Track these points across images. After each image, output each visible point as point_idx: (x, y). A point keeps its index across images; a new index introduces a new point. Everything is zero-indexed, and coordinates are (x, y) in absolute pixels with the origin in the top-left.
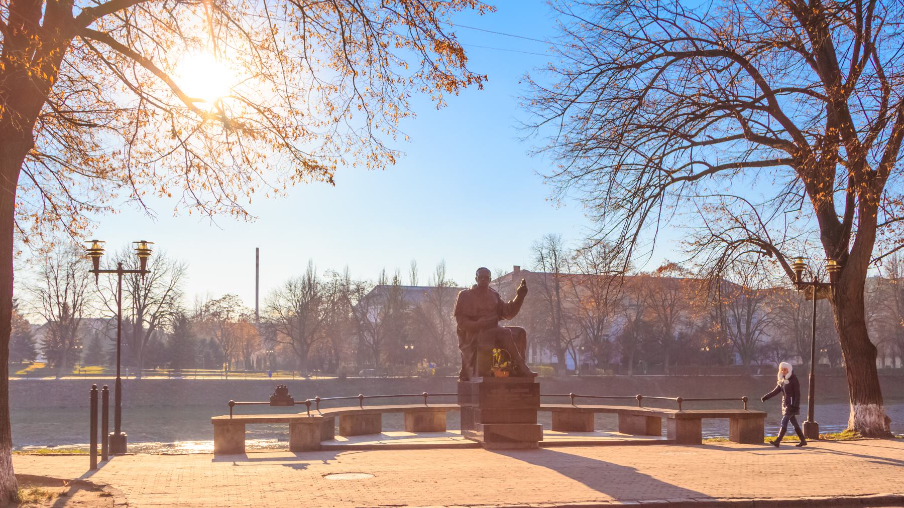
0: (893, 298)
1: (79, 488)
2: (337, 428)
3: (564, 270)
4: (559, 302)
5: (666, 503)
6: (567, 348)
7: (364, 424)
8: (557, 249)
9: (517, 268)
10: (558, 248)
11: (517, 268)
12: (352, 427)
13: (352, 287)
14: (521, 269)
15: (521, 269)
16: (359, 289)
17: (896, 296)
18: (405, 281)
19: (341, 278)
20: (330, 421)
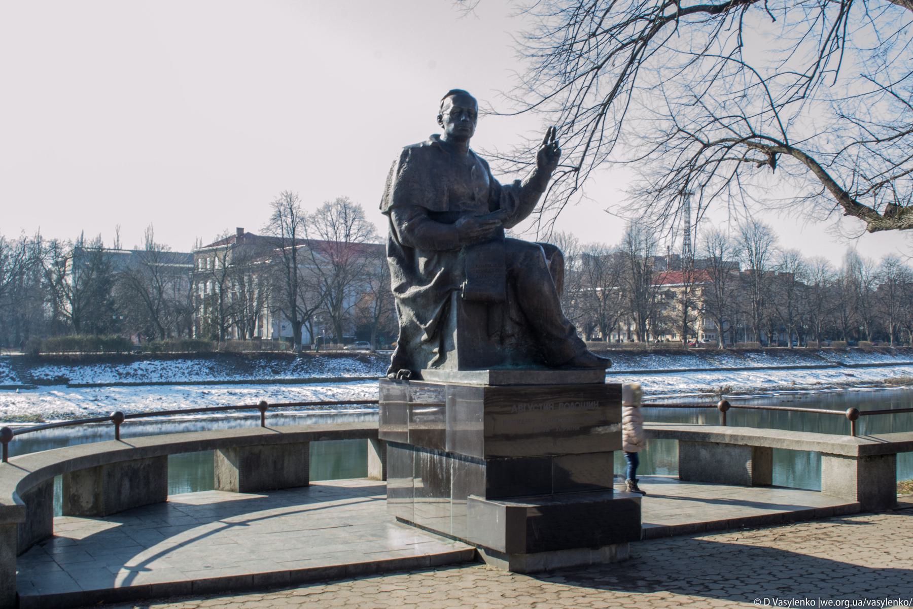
0: (631, 271)
1: (190, 258)
2: (58, 503)
3: (300, 235)
4: (295, 268)
5: (273, 435)
6: (304, 321)
7: (126, 484)
8: (294, 206)
9: (240, 230)
10: (295, 205)
11: (240, 230)
12: (96, 496)
13: (45, 245)
14: (245, 232)
15: (245, 232)
16: (55, 246)
17: (633, 269)
18: (108, 244)
19: (31, 237)
20: (40, 491)
